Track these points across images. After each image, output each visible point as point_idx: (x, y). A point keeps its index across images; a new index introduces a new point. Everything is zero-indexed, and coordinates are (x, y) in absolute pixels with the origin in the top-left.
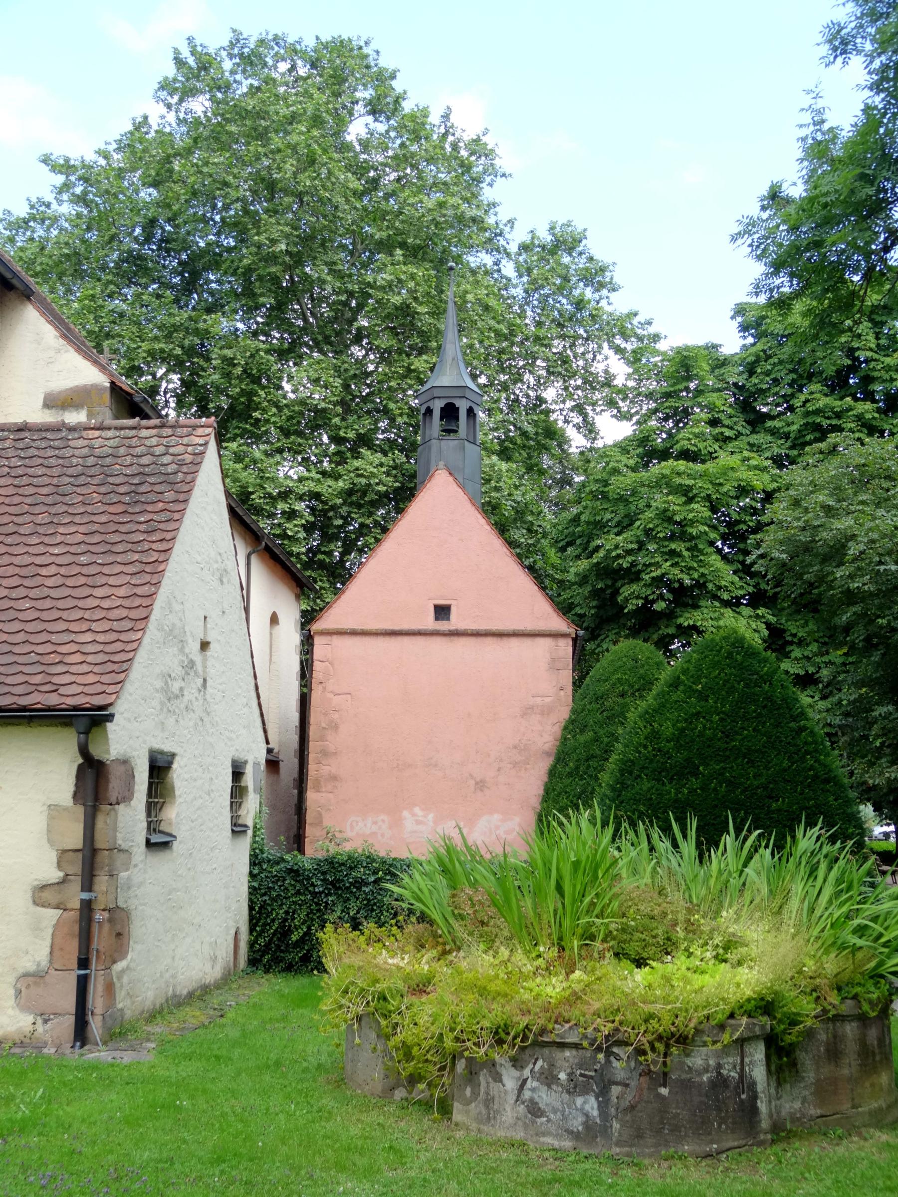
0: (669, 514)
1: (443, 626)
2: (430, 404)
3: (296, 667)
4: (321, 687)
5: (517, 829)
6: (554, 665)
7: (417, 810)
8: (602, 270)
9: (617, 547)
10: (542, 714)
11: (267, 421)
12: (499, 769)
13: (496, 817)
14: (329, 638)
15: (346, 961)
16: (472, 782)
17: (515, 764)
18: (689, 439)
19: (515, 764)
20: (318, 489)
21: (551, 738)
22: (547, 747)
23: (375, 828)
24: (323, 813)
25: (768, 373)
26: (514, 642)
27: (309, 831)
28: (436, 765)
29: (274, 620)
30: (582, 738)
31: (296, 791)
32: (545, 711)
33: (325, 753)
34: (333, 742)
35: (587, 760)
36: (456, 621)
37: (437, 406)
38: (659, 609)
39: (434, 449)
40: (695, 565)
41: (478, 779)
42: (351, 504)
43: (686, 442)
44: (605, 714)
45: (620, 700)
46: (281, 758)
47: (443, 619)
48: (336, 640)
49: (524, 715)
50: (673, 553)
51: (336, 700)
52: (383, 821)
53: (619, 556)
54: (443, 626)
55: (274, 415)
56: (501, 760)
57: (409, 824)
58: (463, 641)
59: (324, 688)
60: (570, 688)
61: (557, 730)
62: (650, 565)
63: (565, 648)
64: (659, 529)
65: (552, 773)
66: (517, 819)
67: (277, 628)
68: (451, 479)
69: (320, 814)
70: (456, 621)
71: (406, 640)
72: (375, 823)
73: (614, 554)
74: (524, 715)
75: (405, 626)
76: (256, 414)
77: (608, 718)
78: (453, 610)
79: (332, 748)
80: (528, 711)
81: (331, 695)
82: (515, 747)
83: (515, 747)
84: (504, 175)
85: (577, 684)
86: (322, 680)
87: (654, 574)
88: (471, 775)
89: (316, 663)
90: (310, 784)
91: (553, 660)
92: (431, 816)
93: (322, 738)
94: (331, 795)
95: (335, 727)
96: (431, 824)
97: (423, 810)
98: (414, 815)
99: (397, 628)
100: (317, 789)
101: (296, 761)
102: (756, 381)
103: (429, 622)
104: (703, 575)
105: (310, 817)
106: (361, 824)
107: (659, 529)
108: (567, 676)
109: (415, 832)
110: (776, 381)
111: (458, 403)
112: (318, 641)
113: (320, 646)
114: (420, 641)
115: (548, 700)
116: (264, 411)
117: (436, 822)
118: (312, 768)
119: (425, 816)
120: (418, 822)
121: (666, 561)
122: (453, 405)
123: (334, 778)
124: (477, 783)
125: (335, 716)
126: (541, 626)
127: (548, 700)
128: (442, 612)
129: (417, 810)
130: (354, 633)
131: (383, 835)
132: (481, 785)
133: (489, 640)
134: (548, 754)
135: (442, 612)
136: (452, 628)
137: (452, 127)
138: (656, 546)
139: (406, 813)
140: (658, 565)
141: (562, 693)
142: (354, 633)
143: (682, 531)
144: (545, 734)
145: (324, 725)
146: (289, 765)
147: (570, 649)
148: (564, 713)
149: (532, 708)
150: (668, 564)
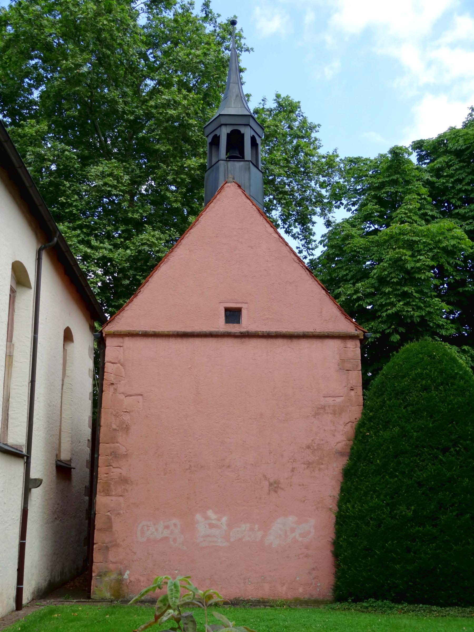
0: (400, 263)
1: (234, 328)
2: (217, 132)
3: (89, 388)
4: (112, 388)
5: (313, 530)
6: (343, 366)
7: (210, 513)
8: (312, 128)
9: (357, 292)
10: (334, 413)
11: (71, 205)
12: (293, 470)
13: (292, 519)
14: (121, 340)
15: (31, 9)
16: (266, 484)
17: (309, 464)
18: (405, 214)
19: (309, 464)
20: (111, 255)
21: (344, 438)
22: (340, 447)
23: (166, 533)
24: (113, 517)
25: (451, 176)
26: (304, 344)
27: (97, 536)
28: (229, 467)
29: (68, 336)
30: (386, 434)
31: (87, 498)
32: (338, 411)
33: (115, 455)
34: (124, 443)
35: (396, 457)
36: (247, 324)
37: (224, 132)
38: (395, 340)
39: (222, 169)
40: (422, 305)
41: (272, 481)
42: (136, 269)
43: (403, 216)
44: (409, 408)
45: (424, 394)
46: (73, 465)
47: (233, 322)
48: (128, 342)
49: (316, 415)
50: (405, 295)
51: (127, 401)
52: (175, 525)
53: (359, 299)
54: (234, 328)
55: (76, 200)
56: (295, 461)
57: (202, 528)
58: (254, 342)
59: (115, 389)
60: (360, 390)
61: (349, 429)
62: (386, 305)
63: (354, 350)
64: (393, 275)
65: (348, 474)
66: (312, 522)
67: (70, 347)
68: (239, 191)
69: (110, 519)
70: (247, 324)
71: (198, 342)
72: (167, 527)
73: (355, 297)
74: (316, 415)
75: (197, 328)
76: (62, 199)
77: (413, 412)
78: (244, 313)
79: (122, 450)
80: (320, 411)
81: (122, 397)
82: (308, 447)
83: (308, 447)
84: (247, 50)
85: (366, 383)
86: (114, 381)
87: (389, 312)
88: (265, 476)
89: (107, 365)
90: (99, 487)
91: (343, 361)
92: (224, 519)
93: (113, 440)
94: (121, 499)
95: (126, 429)
96: (225, 527)
97: (216, 513)
98: (207, 518)
99: (189, 330)
100: (107, 493)
101: (88, 471)
102: (444, 181)
103: (220, 325)
104: (429, 313)
105: (99, 523)
106: (152, 529)
107: (393, 275)
108: (356, 377)
109: (209, 536)
110: (460, 181)
111: (243, 130)
112: (109, 342)
113: (112, 349)
114: (212, 343)
115: (339, 400)
116: (68, 197)
117: (230, 526)
118: (102, 470)
119: (219, 520)
120: (211, 526)
121: (399, 301)
122: (239, 131)
123: (124, 481)
124: (271, 484)
125: (126, 417)
126: (330, 328)
127: (339, 400)
128: (233, 315)
129: (210, 513)
130: (146, 335)
131: (175, 540)
132: (275, 486)
133: (280, 342)
134: (341, 454)
135: (233, 315)
136: (243, 330)
137: (211, 13)
138: (390, 289)
139: (198, 517)
140: (393, 305)
141: (353, 393)
142: (146, 335)
143: (410, 277)
144: (337, 433)
145: (114, 427)
146: (80, 473)
147: (359, 351)
148: (355, 413)
149: (323, 408)
150: (401, 303)
